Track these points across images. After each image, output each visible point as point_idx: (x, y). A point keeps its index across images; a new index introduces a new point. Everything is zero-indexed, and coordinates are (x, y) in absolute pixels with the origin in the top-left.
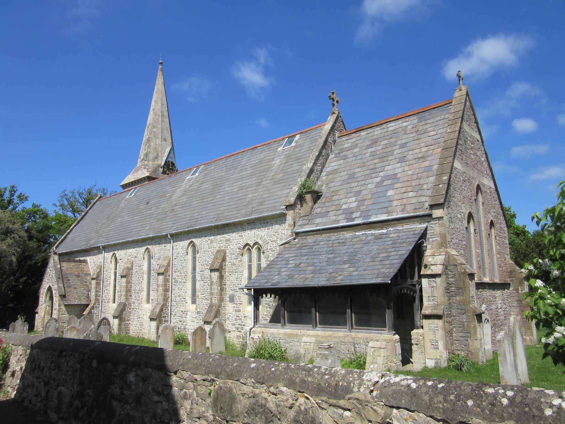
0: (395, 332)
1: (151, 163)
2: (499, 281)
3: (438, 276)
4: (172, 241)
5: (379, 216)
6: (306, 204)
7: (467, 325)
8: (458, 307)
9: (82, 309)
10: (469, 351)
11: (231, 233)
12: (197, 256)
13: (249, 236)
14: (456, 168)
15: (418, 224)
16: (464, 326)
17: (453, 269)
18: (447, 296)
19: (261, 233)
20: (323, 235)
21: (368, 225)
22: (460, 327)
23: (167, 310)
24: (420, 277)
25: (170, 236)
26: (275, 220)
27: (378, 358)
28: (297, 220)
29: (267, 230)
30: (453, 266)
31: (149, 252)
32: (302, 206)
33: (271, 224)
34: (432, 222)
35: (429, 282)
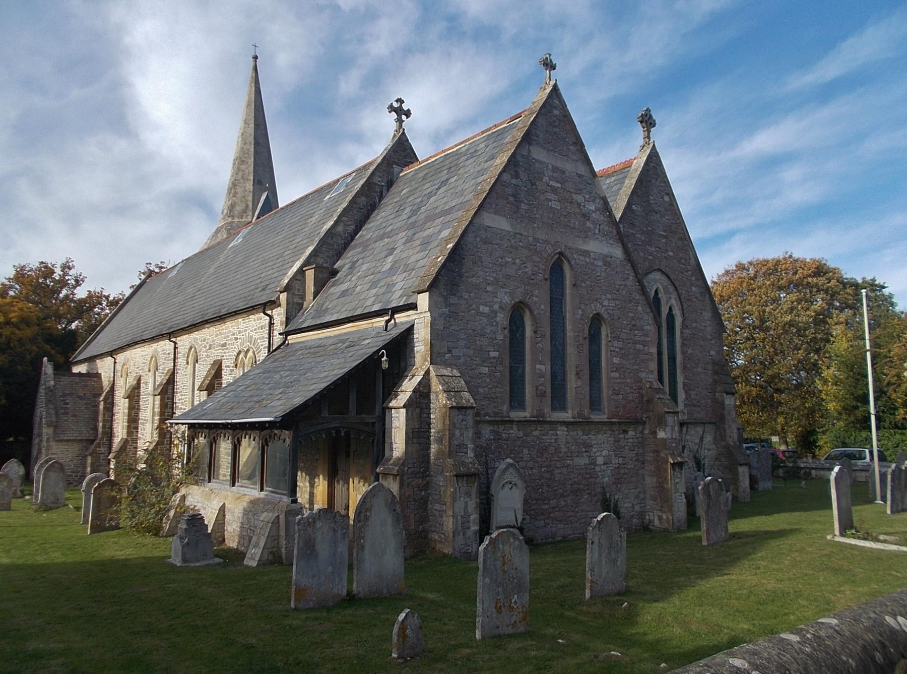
1: (236, 220)
2: (607, 418)
9: (85, 446)
14: (489, 227)
29: (260, 330)
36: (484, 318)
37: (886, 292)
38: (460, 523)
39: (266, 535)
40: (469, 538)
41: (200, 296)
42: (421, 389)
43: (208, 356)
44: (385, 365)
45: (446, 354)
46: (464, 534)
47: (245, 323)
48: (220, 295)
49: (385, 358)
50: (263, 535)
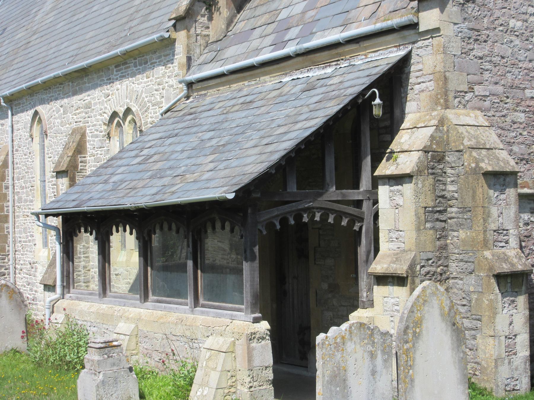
0: (260, 315)
3: (407, 180)
4: (10, 113)
5: (327, 32)
6: (218, 13)
7: (477, 299)
8: (461, 257)
10: (478, 363)
11: (92, 89)
12: (47, 142)
13: (118, 93)
15: (395, 49)
16: (470, 301)
17: (454, 162)
18: (433, 228)
19: (137, 86)
20: (234, 86)
21: (304, 58)
22: (464, 305)
23: (6, 260)
24: (376, 182)
25: (4, 102)
26: (158, 54)
27: (212, 372)
28: (198, 51)
29: (145, 80)
30: (457, 153)
31: (40, 121)
32: (210, 19)
33: (151, 64)
34: (420, 44)
35: (391, 195)
36: (516, 38)
37: (79, 234)
38: (503, 346)
39: (219, 368)
40: (516, 369)
41: (38, 41)
42: (434, 146)
43: (62, 124)
44: (377, 112)
45: (466, 92)
46: (509, 363)
47: (119, 71)
48: (71, 37)
49: (378, 101)
50: (214, 369)
